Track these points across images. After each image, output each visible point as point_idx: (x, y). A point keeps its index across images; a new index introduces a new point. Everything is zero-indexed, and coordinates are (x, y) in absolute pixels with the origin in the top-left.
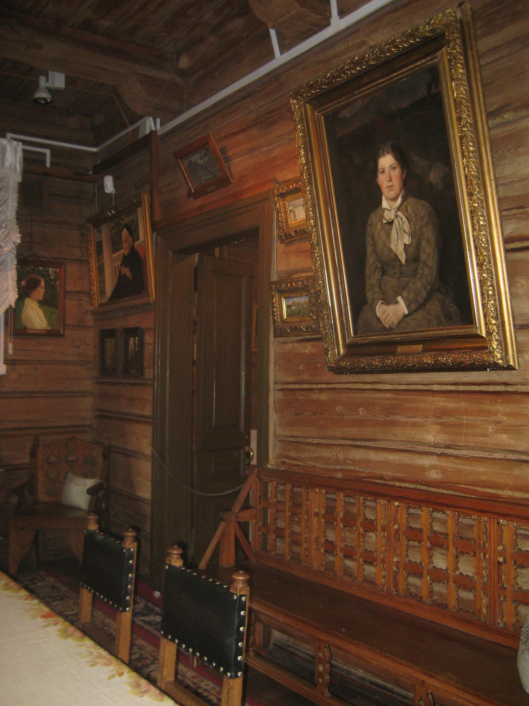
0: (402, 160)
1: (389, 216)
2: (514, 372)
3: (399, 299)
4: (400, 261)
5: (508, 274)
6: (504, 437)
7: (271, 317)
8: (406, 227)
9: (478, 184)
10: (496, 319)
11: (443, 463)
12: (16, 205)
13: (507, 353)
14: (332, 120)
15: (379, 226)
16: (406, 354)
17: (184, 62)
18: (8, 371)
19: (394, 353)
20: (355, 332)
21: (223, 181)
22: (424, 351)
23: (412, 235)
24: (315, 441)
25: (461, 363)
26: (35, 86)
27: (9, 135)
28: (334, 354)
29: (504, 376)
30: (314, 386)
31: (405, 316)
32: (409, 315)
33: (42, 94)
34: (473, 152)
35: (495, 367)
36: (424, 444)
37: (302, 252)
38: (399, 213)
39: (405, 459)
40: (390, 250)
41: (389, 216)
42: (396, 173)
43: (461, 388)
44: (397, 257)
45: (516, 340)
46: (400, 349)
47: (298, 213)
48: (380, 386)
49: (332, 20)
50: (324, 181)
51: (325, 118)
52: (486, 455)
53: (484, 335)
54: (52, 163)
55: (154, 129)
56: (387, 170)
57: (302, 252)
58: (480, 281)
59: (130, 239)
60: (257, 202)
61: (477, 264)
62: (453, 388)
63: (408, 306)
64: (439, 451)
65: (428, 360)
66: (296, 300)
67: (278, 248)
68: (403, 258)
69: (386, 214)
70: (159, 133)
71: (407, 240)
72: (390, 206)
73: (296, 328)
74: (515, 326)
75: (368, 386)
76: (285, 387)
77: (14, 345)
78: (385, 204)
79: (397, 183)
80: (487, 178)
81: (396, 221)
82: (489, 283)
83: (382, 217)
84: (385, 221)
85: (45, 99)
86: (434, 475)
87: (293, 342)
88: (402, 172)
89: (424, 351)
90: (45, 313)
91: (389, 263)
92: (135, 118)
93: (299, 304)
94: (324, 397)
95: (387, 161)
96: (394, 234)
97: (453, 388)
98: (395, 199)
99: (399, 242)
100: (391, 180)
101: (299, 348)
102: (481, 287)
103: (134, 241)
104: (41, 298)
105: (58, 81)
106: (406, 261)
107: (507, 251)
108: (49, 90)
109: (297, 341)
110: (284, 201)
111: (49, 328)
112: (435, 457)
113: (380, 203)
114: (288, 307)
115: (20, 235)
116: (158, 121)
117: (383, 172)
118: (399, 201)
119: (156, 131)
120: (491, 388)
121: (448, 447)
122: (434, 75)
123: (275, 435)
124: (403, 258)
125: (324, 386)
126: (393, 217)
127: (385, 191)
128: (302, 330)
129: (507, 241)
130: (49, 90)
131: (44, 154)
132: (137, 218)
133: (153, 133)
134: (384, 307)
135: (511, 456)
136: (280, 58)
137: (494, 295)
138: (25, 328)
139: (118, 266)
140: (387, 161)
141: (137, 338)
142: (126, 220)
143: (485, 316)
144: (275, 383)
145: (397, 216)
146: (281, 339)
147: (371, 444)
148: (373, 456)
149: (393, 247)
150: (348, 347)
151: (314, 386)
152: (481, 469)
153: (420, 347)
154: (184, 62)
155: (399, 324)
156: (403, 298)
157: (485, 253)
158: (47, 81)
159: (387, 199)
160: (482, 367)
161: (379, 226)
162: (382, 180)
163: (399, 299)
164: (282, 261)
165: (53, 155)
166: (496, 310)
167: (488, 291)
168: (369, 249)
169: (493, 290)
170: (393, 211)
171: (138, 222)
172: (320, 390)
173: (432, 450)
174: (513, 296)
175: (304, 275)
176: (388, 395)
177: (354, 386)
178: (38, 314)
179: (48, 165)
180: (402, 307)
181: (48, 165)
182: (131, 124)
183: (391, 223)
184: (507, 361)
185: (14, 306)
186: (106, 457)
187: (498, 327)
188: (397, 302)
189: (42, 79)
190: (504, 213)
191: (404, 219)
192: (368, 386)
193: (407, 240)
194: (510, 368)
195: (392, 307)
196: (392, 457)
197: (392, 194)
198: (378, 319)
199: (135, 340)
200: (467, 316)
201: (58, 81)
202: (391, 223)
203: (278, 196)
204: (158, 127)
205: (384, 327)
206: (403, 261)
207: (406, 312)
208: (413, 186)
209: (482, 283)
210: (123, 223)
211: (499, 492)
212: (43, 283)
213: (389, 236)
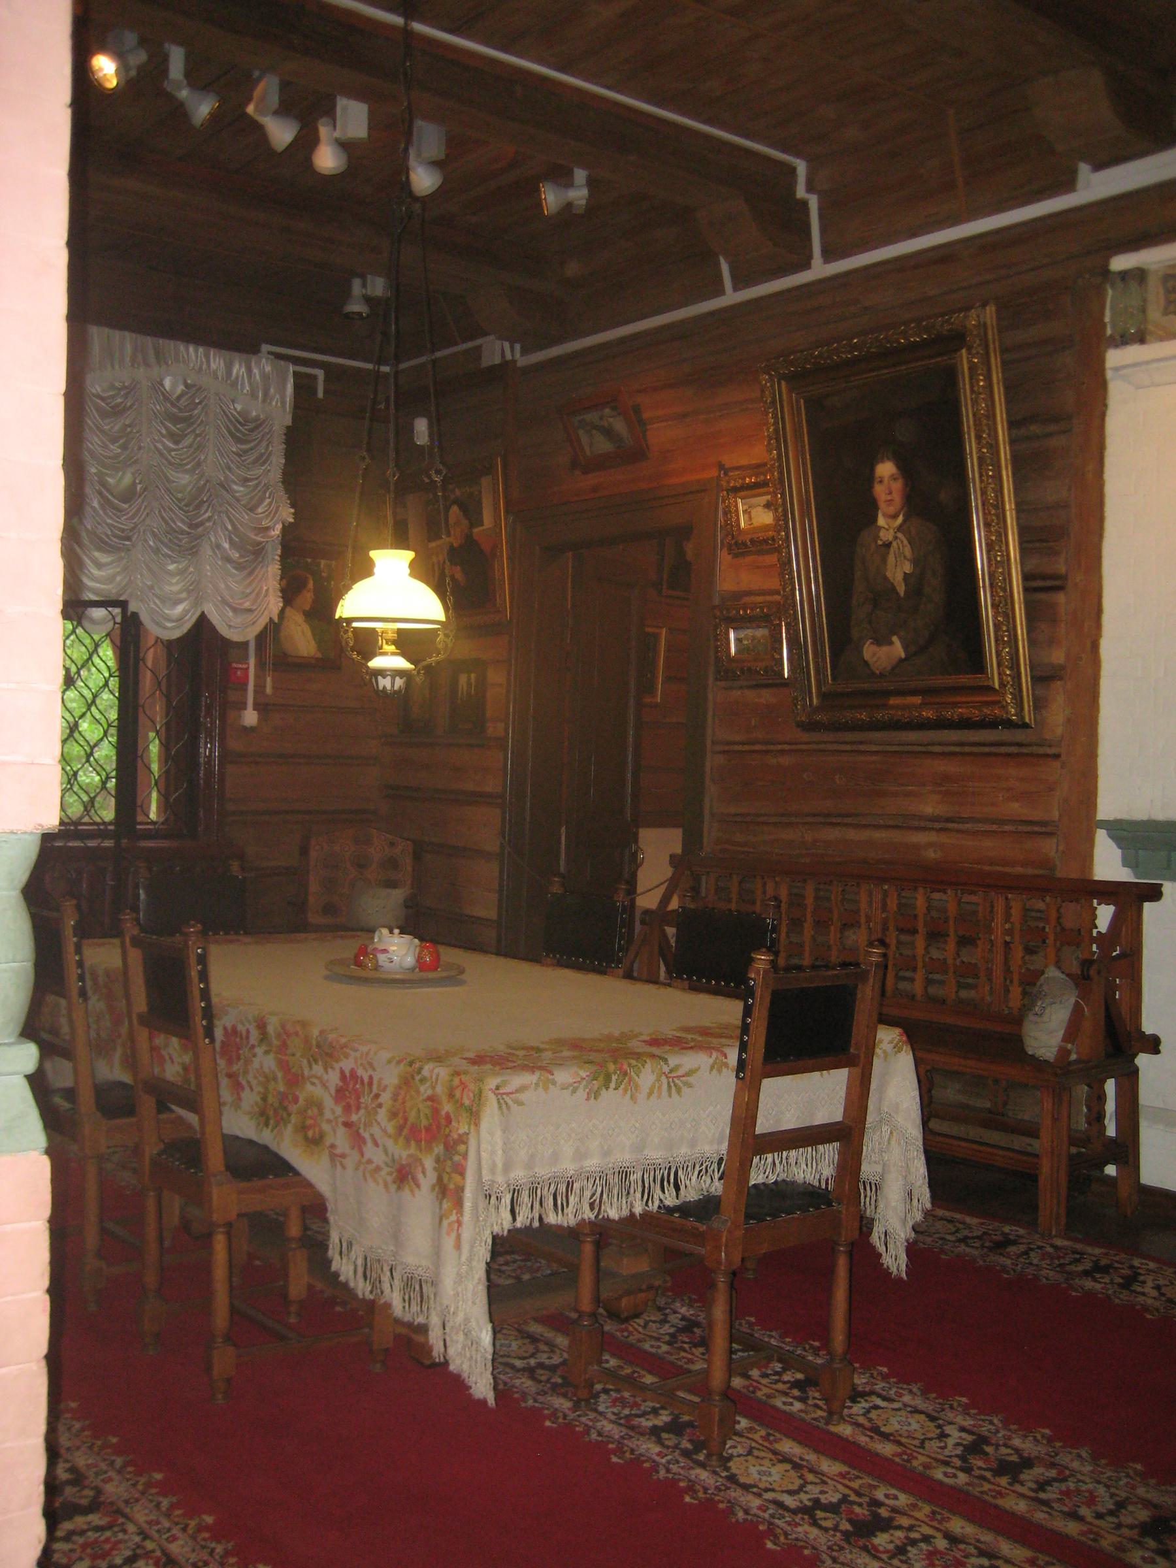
0: (906, 470)
1: (886, 536)
2: (1029, 731)
3: (895, 639)
4: (897, 593)
5: (1027, 618)
6: (1016, 805)
7: (712, 653)
8: (908, 551)
9: (988, 425)
10: (1011, 669)
11: (944, 839)
12: (283, 461)
13: (1022, 709)
14: (815, 406)
15: (873, 546)
16: (897, 707)
17: (573, 269)
18: (259, 720)
19: (885, 706)
20: (834, 679)
21: (635, 454)
22: (924, 704)
23: (915, 562)
24: (772, 820)
25: (968, 719)
26: (345, 293)
27: (265, 348)
28: (804, 706)
29: (1019, 736)
30: (772, 747)
31: (901, 661)
32: (906, 659)
33: (356, 307)
34: (991, 477)
35: (1009, 724)
36: (921, 818)
37: (758, 567)
38: (900, 535)
39: (895, 836)
40: (886, 578)
41: (886, 536)
42: (897, 486)
43: (967, 749)
44: (893, 589)
45: (1033, 694)
46: (893, 701)
47: (753, 515)
48: (862, 748)
49: (813, 262)
50: (800, 482)
51: (805, 402)
52: (995, 827)
53: (997, 686)
54: (326, 392)
55: (509, 357)
56: (886, 481)
57: (758, 567)
58: (995, 625)
59: (465, 522)
60: (691, 493)
61: (993, 605)
62: (958, 749)
63: (906, 647)
64: (938, 825)
65: (928, 714)
66: (749, 632)
67: (724, 558)
68: (901, 590)
69: (882, 534)
70: (519, 364)
71: (908, 568)
72: (887, 524)
73: (749, 669)
74: (1032, 678)
75: (848, 747)
76: (727, 748)
77: (273, 681)
78: (881, 521)
79: (897, 498)
80: (1004, 473)
81: (894, 544)
82: (1005, 628)
83: (877, 537)
84: (880, 542)
85: (360, 314)
86: (931, 854)
87: (741, 688)
88: (906, 485)
89: (924, 704)
90: (313, 630)
91: (882, 594)
92: (476, 332)
93: (754, 638)
94: (785, 761)
95: (886, 469)
96: (891, 559)
97: (958, 749)
98: (895, 517)
99: (898, 569)
100: (890, 493)
101: (751, 696)
102: (996, 632)
103: (472, 526)
104: (307, 608)
105: (378, 286)
106: (906, 592)
107: (1026, 590)
108: (368, 300)
109: (749, 687)
110: (735, 497)
111: (319, 655)
112: (934, 833)
113: (876, 520)
114: (738, 641)
115: (292, 510)
116: (518, 347)
117: (881, 482)
118: (900, 519)
119: (514, 361)
120: (1003, 750)
121: (948, 820)
122: (951, 375)
123: (712, 815)
124: (901, 590)
125: (786, 747)
126: (891, 539)
127: (882, 505)
128: (758, 673)
129: (1027, 577)
130: (368, 300)
131: (315, 377)
132: (480, 492)
133: (505, 365)
134: (874, 648)
135: (1022, 828)
136: (731, 297)
137: (1009, 641)
138: (285, 655)
139: (439, 563)
140: (886, 469)
141: (473, 676)
142: (458, 492)
143: (999, 665)
144: (713, 742)
145: (896, 538)
146: (723, 684)
147: (848, 820)
148: (852, 834)
149: (889, 574)
150: (823, 696)
151: (772, 747)
152: (988, 843)
153: (917, 700)
154: (573, 269)
155: (893, 669)
156: (899, 638)
157: (993, 512)
158: (364, 285)
159: (884, 515)
160: (993, 724)
161: (873, 546)
162: (879, 491)
163: (895, 639)
164: (732, 577)
165: (327, 379)
166: (1011, 659)
167: (1003, 637)
168: (858, 574)
169: (1009, 636)
170: (891, 531)
171: (480, 499)
172: (782, 752)
173: (929, 824)
174: (1032, 642)
175: (760, 599)
176: (874, 758)
177: (830, 747)
178: (303, 632)
179: (320, 395)
180: (897, 649)
181: (320, 395)
182: (465, 340)
183: (888, 545)
184: (1023, 718)
185: (276, 620)
186: (417, 857)
187: (1013, 679)
188: (891, 643)
189: (356, 283)
190: (1024, 545)
191: (906, 542)
192: (848, 747)
193: (908, 568)
194: (1026, 726)
195: (885, 649)
196: (877, 835)
197: (891, 510)
198: (866, 663)
199: (469, 678)
200: (977, 663)
201: (378, 286)
202: (888, 545)
203: (728, 491)
204: (518, 355)
205: (873, 673)
206: (902, 594)
207: (903, 655)
208: (917, 503)
209: (997, 626)
210: (452, 497)
211: (1008, 870)
212: (311, 585)
213: (884, 560)
